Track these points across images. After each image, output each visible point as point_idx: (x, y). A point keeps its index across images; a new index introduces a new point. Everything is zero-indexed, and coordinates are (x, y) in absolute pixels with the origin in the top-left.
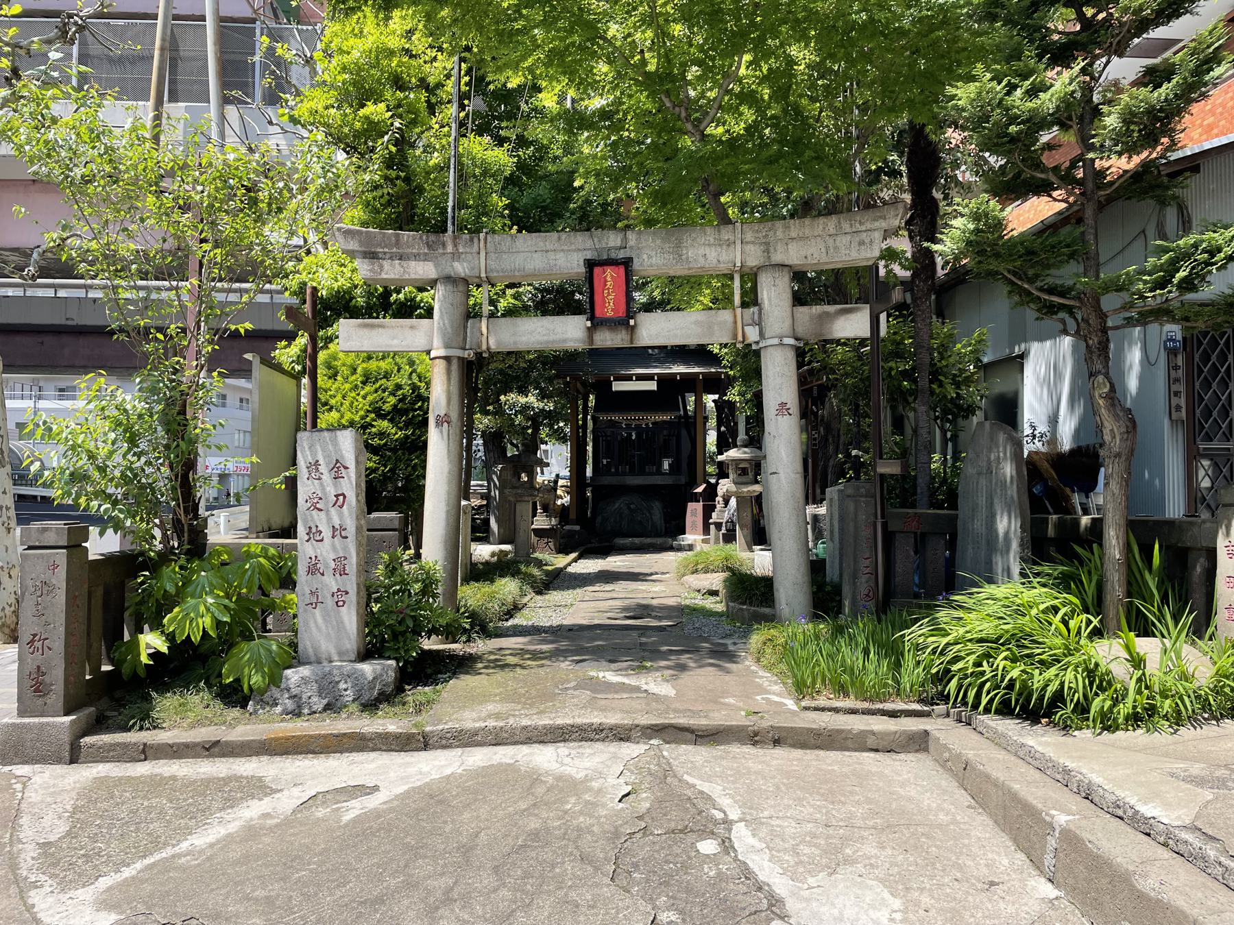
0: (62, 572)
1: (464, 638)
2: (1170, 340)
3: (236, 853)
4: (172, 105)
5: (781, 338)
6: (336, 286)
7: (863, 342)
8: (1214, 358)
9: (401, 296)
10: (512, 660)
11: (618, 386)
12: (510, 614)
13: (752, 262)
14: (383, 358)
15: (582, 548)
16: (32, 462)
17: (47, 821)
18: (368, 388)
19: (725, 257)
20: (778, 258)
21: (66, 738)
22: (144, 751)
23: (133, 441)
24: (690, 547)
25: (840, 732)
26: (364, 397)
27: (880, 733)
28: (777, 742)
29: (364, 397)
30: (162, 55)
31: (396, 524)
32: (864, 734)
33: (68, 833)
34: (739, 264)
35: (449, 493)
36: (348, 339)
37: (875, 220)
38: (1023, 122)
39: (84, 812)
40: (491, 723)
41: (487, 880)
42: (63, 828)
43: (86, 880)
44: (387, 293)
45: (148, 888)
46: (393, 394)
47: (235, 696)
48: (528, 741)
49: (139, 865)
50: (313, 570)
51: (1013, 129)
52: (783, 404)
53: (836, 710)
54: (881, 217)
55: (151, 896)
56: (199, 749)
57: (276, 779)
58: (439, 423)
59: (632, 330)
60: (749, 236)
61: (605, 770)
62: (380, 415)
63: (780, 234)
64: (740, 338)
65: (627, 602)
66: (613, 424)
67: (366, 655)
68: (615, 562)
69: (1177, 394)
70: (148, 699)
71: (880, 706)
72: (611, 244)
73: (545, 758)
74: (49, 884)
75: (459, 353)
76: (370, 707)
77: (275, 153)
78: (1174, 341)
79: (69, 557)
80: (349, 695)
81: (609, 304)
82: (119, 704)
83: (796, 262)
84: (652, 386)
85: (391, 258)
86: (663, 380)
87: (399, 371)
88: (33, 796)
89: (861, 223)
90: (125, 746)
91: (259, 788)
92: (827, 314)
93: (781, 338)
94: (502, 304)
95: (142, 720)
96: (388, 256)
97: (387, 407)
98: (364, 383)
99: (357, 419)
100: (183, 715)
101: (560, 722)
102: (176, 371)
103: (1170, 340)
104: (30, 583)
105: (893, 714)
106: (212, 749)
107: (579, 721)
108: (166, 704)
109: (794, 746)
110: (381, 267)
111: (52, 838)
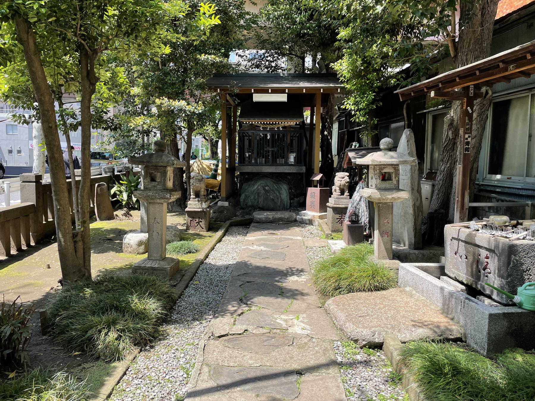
11: (257, 98)
15: (228, 223)
24: (310, 222)
66: (254, 127)
84: (283, 98)
96: (229, 112)
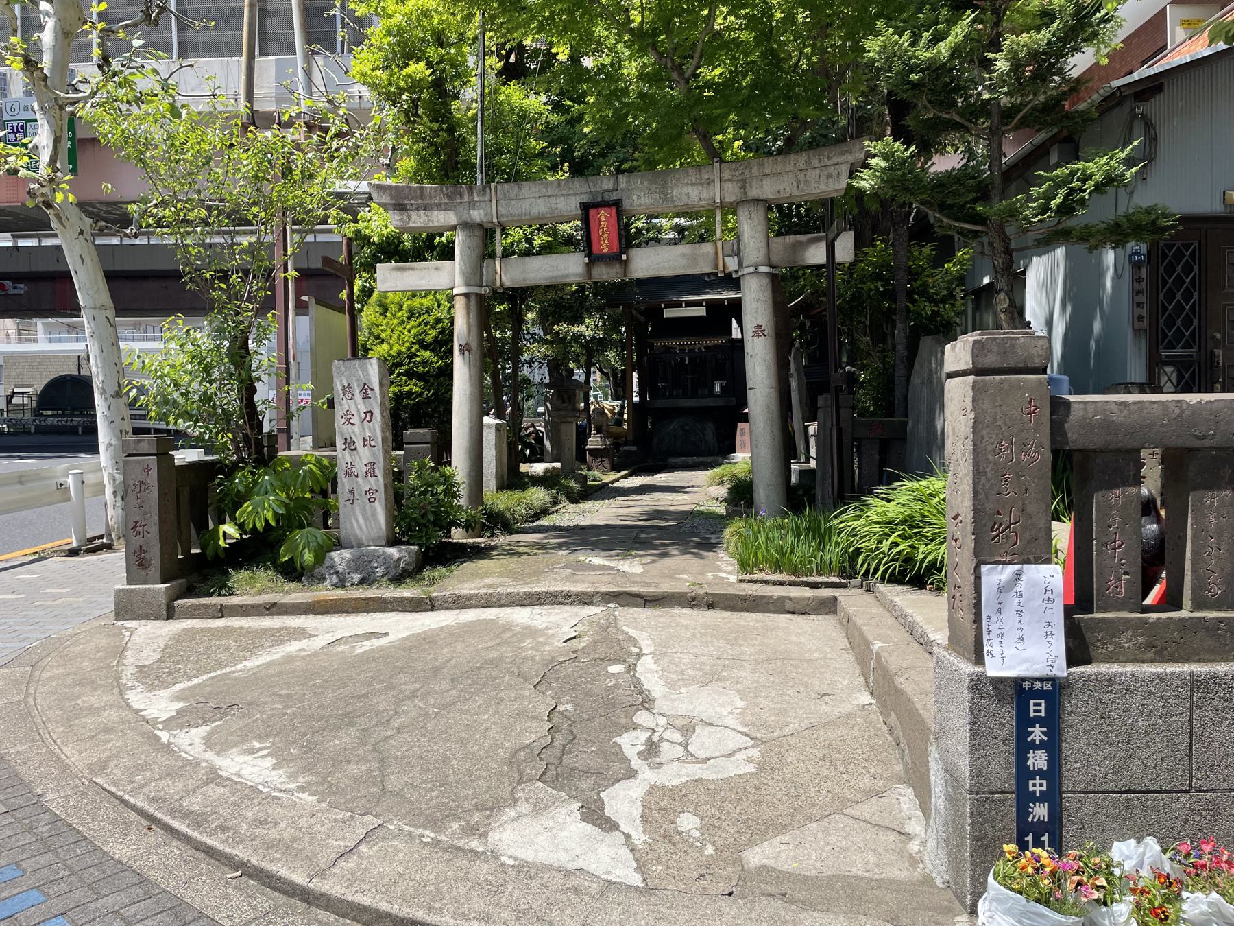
0: (154, 474)
1: (488, 534)
2: (1134, 254)
3: (276, 669)
4: (263, 58)
5: (756, 266)
6: (385, 232)
7: (822, 266)
8: (1179, 269)
9: (444, 239)
10: (522, 549)
11: (669, 313)
12: (537, 517)
13: (730, 198)
14: (426, 296)
16: (130, 390)
17: (145, 654)
18: (412, 323)
19: (705, 195)
20: (754, 193)
21: (163, 600)
22: (221, 611)
23: (207, 369)
25: (763, 597)
26: (409, 331)
27: (796, 598)
28: (711, 606)
29: (409, 331)
30: (251, 11)
31: (428, 439)
32: (782, 599)
33: (159, 660)
34: (718, 201)
35: (471, 411)
36: (384, 281)
37: (842, 154)
38: (922, 71)
39: (170, 649)
40: (483, 591)
41: (445, 685)
42: (156, 656)
43: (165, 685)
44: (431, 237)
45: (208, 689)
46: (433, 327)
47: (292, 572)
48: (512, 604)
49: (205, 677)
50: (349, 474)
51: (913, 77)
52: (758, 327)
53: (767, 582)
54: (847, 152)
55: (210, 693)
56: (262, 609)
57: (316, 629)
58: (462, 352)
59: (626, 264)
60: (727, 175)
61: (561, 622)
62: (423, 346)
63: (755, 171)
64: (721, 268)
65: (646, 508)
67: (393, 541)
68: (661, 479)
69: (1139, 305)
70: (227, 574)
71: (804, 579)
72: (605, 187)
73: (521, 616)
74: (140, 687)
75: (476, 290)
76: (398, 579)
77: (358, 100)
78: (1138, 254)
79: (159, 462)
80: (380, 572)
81: (605, 240)
82: (205, 579)
83: (770, 196)
84: (702, 311)
85: (417, 209)
86: (710, 305)
87: (439, 306)
88: (136, 638)
89: (829, 158)
90: (206, 606)
91: (302, 634)
92: (800, 243)
93: (756, 266)
94: (537, 242)
95: (220, 588)
97: (429, 339)
98: (409, 318)
99: (403, 350)
100: (251, 585)
101: (536, 589)
102: (237, 313)
103: (1134, 254)
104: (131, 482)
105: (815, 586)
106: (271, 609)
107: (552, 589)
108: (239, 577)
109: (725, 609)
110: (409, 217)
111: (147, 663)
